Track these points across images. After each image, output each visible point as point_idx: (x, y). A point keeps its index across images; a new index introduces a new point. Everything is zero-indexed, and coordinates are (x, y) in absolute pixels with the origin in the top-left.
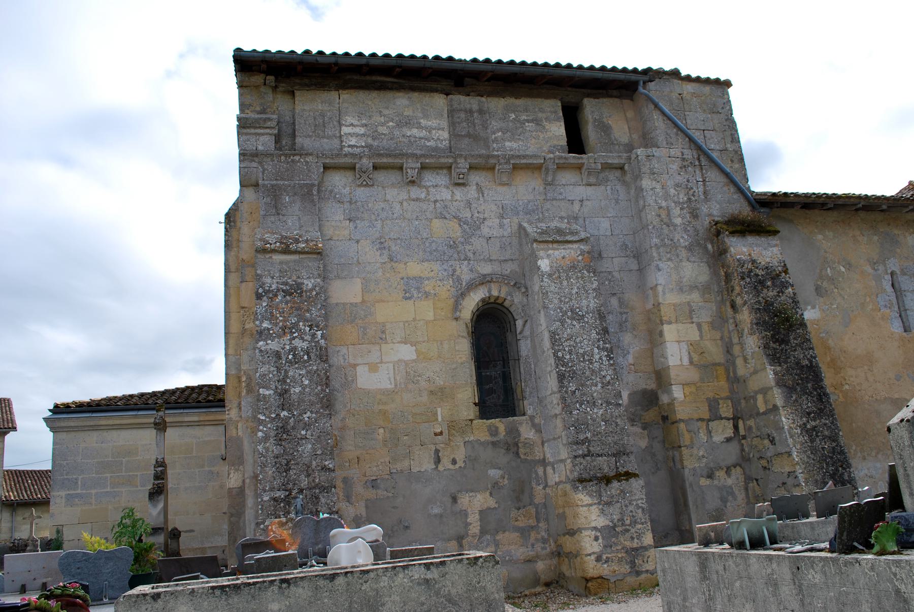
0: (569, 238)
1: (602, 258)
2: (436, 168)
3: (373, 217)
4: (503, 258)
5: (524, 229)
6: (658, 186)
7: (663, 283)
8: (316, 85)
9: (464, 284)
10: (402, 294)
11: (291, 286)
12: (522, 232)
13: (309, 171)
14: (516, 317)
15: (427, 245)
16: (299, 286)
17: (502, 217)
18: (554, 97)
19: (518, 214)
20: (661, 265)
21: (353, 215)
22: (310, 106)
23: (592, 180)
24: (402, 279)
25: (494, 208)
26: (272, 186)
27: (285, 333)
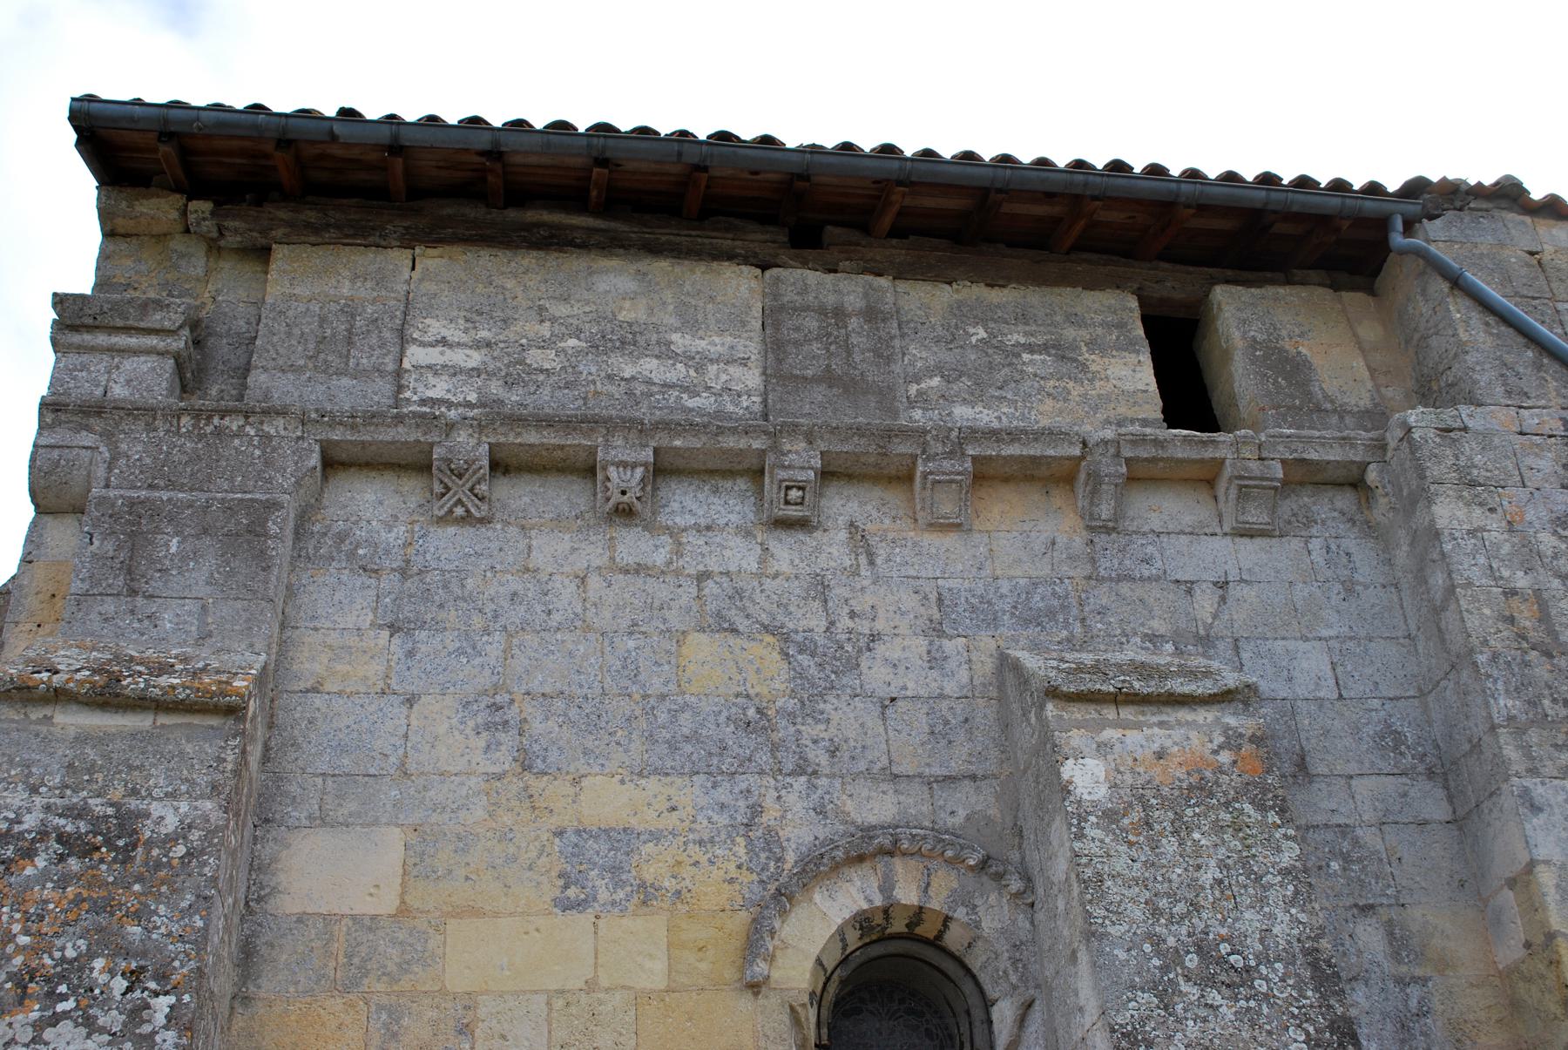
0: (1180, 686)
1: (1310, 778)
2: (712, 472)
3: (477, 621)
4: (937, 771)
5: (1016, 667)
6: (1494, 524)
7: (1557, 857)
8: (338, 227)
9: (791, 858)
10: (551, 890)
11: (97, 822)
12: (1010, 678)
13: (267, 463)
14: (992, 993)
15: (663, 717)
16: (127, 822)
17: (936, 630)
18: (1118, 285)
19: (995, 622)
20: (1540, 791)
21: (407, 611)
22: (312, 282)
23: (1256, 516)
24: (560, 833)
25: (910, 602)
26: (132, 504)
27: (22, 998)
